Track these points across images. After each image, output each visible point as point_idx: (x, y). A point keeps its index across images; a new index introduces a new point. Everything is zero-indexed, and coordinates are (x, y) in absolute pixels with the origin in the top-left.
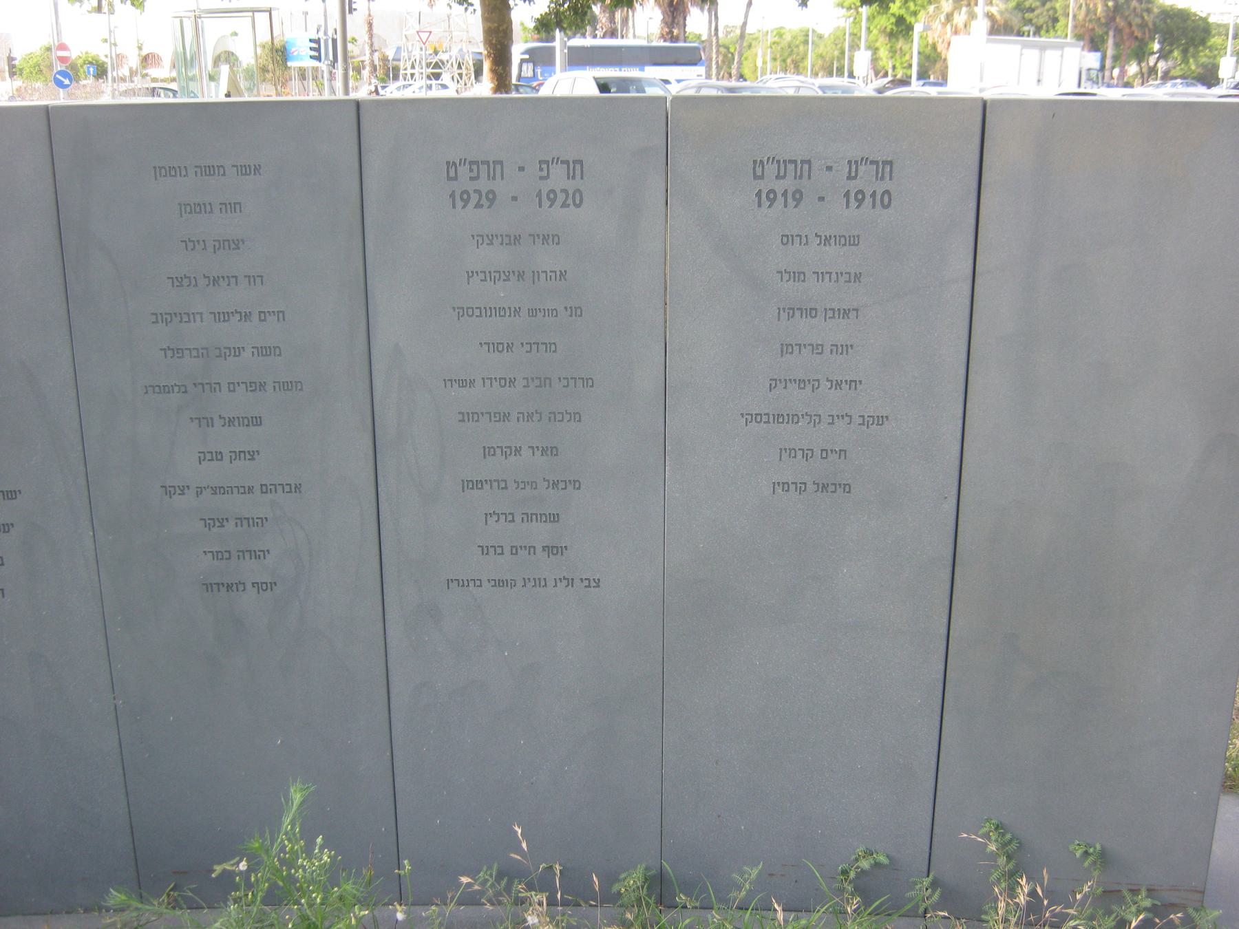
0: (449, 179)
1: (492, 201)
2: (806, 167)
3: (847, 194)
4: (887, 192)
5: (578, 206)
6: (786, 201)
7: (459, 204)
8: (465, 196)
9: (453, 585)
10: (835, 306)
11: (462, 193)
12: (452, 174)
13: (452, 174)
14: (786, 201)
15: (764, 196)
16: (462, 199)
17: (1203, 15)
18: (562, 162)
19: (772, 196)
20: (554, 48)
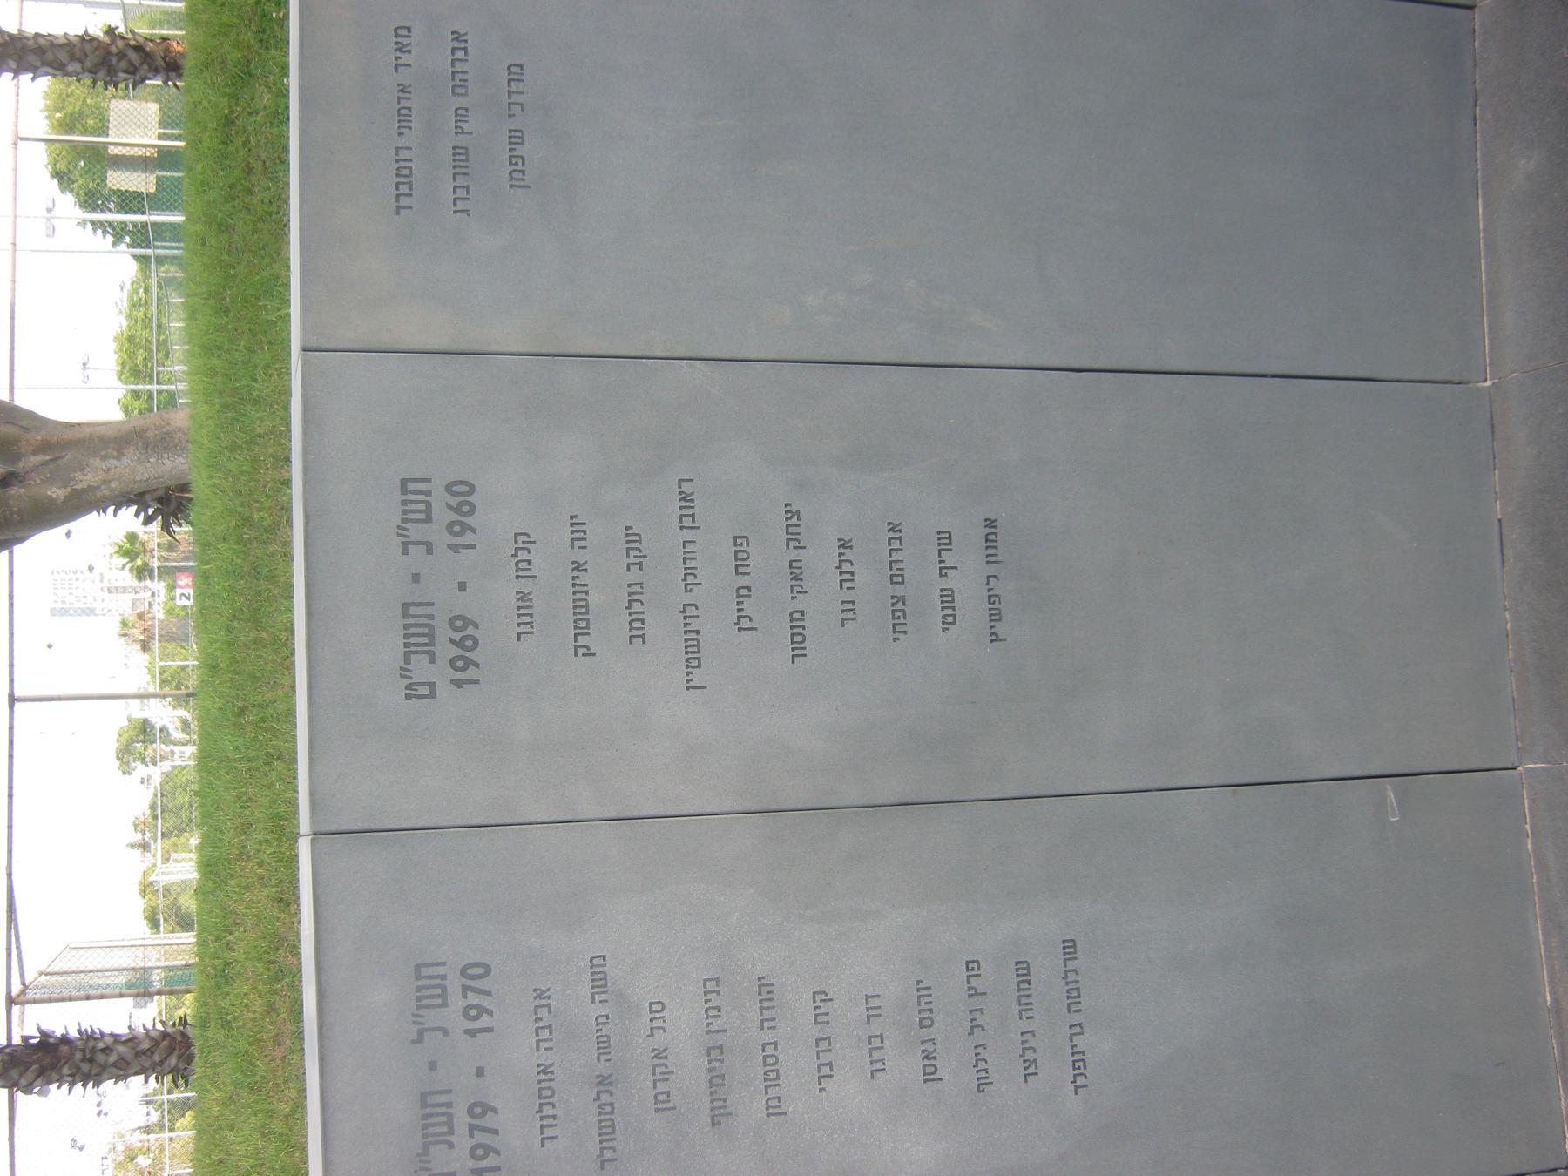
0: (433, 695)
1: (468, 622)
2: (413, 610)
3: (455, 548)
4: (448, 488)
5: (488, 970)
6: (470, 682)
7: (485, 1021)
8: (473, 1012)
9: (1000, 629)
10: (594, 1149)
11: (452, 533)
12: (425, 690)
13: (425, 690)
14: (470, 682)
15: (477, 1025)
16: (484, 1157)
17: (81, 32)
18: (407, 661)
19: (459, 623)
20: (160, 392)
